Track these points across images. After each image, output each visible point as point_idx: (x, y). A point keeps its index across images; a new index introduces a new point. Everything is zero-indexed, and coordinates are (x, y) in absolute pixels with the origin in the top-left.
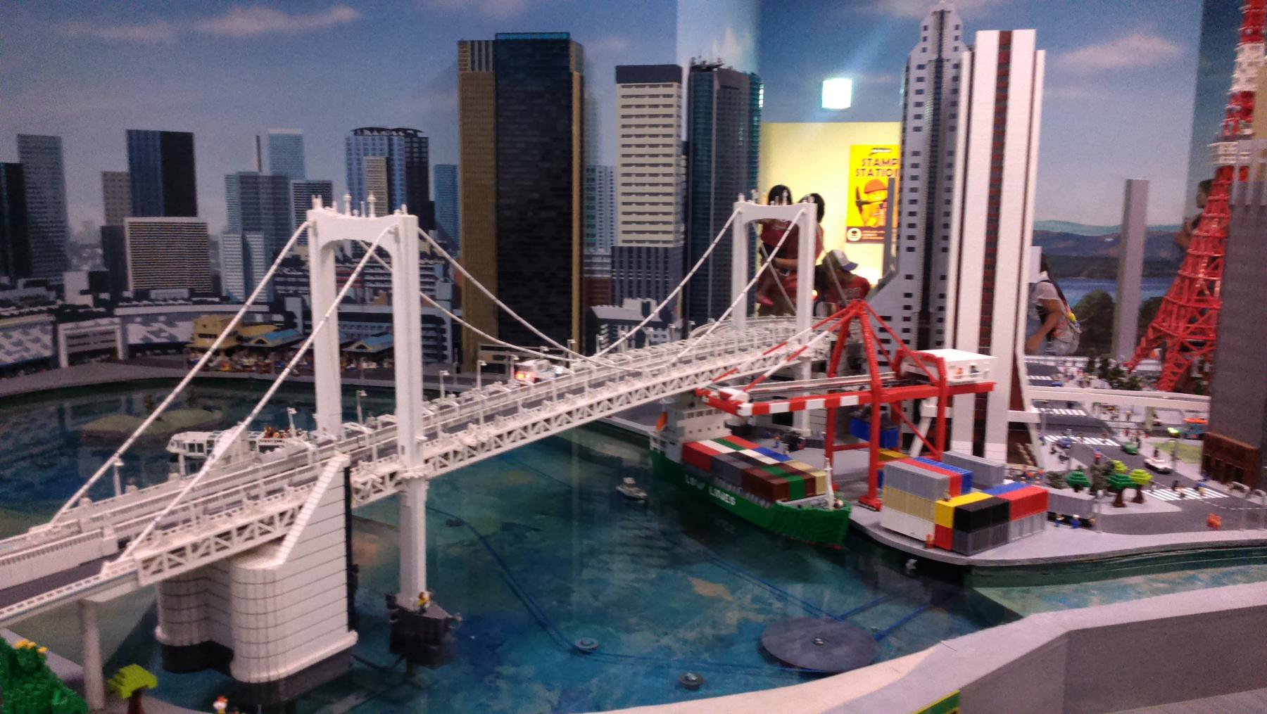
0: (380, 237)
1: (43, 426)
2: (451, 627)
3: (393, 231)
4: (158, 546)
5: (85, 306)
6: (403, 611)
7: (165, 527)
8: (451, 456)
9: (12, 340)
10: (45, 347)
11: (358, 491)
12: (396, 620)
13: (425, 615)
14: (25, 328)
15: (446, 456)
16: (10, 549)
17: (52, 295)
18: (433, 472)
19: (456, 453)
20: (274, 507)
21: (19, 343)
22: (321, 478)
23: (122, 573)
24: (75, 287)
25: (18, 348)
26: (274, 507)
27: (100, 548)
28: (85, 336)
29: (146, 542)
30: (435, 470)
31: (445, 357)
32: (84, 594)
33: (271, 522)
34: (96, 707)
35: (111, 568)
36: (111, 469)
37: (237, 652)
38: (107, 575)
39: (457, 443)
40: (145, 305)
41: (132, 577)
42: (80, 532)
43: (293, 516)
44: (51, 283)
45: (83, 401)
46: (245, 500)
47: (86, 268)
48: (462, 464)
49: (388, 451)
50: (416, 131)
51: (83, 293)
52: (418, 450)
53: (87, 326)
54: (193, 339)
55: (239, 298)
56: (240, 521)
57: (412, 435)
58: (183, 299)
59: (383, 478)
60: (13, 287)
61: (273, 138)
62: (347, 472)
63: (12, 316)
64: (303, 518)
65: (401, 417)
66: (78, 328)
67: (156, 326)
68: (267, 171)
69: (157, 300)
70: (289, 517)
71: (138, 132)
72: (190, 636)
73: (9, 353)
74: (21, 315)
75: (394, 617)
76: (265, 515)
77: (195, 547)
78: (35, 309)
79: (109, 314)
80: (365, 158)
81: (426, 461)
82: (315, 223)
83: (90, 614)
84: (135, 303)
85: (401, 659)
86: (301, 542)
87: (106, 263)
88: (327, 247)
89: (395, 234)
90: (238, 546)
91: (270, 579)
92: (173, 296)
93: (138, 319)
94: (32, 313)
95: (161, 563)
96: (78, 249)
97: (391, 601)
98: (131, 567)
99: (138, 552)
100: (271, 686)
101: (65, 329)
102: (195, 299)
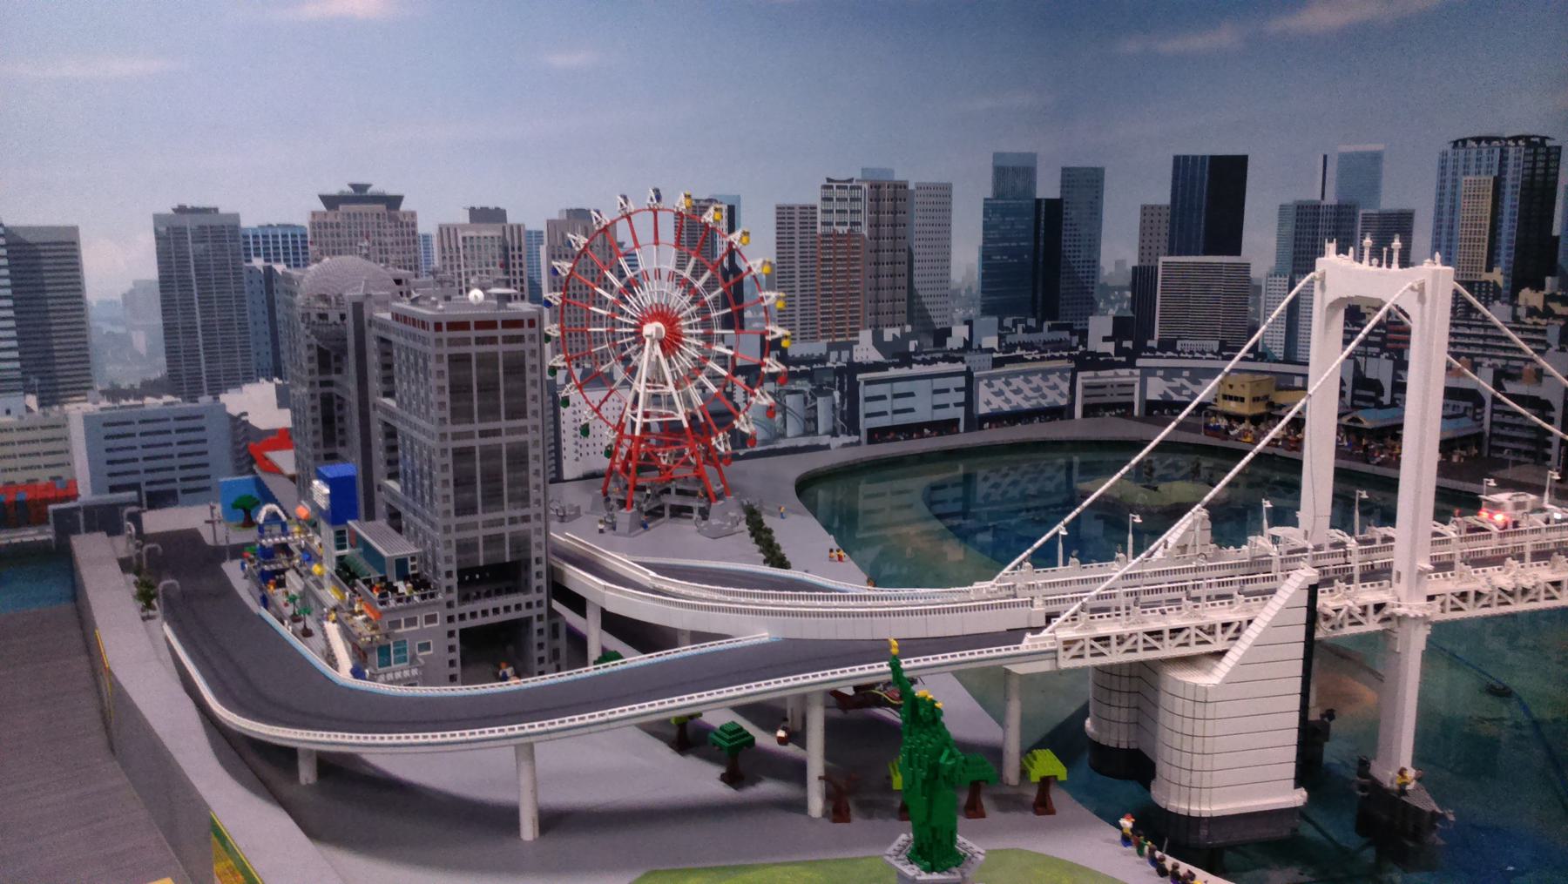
0: (1397, 295)
1: (1051, 479)
2: (1438, 825)
3: (1416, 287)
4: (1080, 629)
5: (1108, 354)
6: (1376, 786)
7: (1093, 610)
8: (1472, 596)
9: (992, 390)
10: (1062, 395)
11: (1327, 618)
12: (1366, 794)
13: (1404, 798)
14: (1046, 373)
15: (1463, 596)
16: (949, 599)
17: (1076, 339)
18: (1435, 612)
19: (1478, 595)
20: (1218, 614)
21: (1038, 389)
22: (1279, 592)
23: (1039, 649)
24: (1099, 328)
25: (1036, 394)
26: (1218, 614)
27: (1029, 618)
28: (1103, 386)
29: (1070, 622)
30: (1443, 611)
31: (1548, 458)
32: (1006, 661)
33: (1211, 631)
34: (1010, 783)
35: (1031, 640)
36: (1057, 534)
37: (1161, 768)
38: (1027, 647)
39: (1483, 581)
40: (1168, 357)
41: (1053, 655)
42: (1015, 597)
43: (1238, 630)
44: (1075, 328)
45: (1091, 457)
46: (1184, 599)
47: (1112, 312)
48: (1487, 612)
49: (1374, 575)
50: (1543, 139)
51: (1105, 339)
52: (1418, 581)
53: (1106, 376)
54: (1216, 400)
55: (1277, 355)
56: (1176, 622)
57: (1413, 560)
58: (1212, 352)
59: (1365, 608)
60: (1039, 329)
61: (1345, 158)
62: (1313, 591)
63: (1034, 360)
64: (1251, 634)
65: (1400, 532)
66: (1096, 377)
67: (1177, 382)
68: (1331, 199)
69: (1182, 351)
70: (1235, 630)
71: (1186, 158)
72: (1116, 737)
73: (1027, 399)
74: (1042, 359)
75: (1363, 788)
76: (1205, 622)
77: (1121, 640)
78: (1057, 354)
79: (1130, 364)
80: (1464, 178)
81: (1431, 598)
82: (1323, 274)
83: (1014, 683)
84: (1158, 354)
85: (1369, 844)
86: (1242, 663)
87: (1133, 309)
88: (1334, 306)
89: (1420, 291)
90: (1168, 650)
91: (1202, 698)
92: (1200, 348)
93: (1160, 373)
94: (1053, 358)
95: (1082, 648)
96: (1107, 290)
97: (1364, 765)
98: (1052, 644)
99: (1062, 631)
100: (1198, 821)
101: (1083, 377)
102: (1225, 353)
